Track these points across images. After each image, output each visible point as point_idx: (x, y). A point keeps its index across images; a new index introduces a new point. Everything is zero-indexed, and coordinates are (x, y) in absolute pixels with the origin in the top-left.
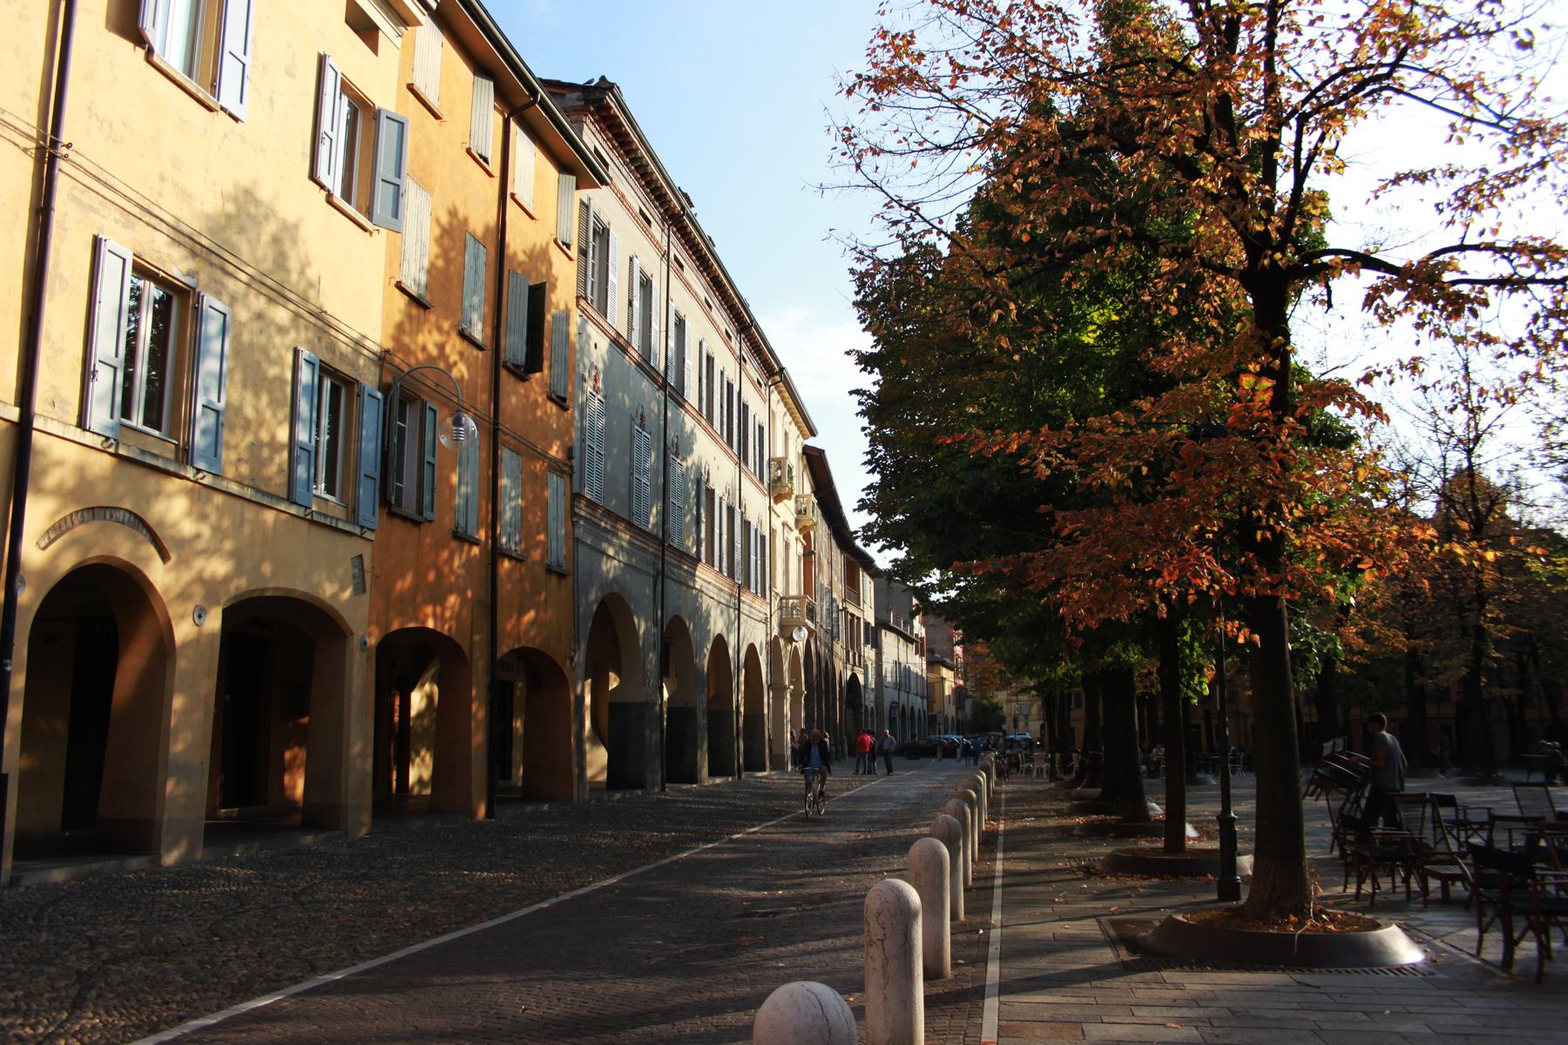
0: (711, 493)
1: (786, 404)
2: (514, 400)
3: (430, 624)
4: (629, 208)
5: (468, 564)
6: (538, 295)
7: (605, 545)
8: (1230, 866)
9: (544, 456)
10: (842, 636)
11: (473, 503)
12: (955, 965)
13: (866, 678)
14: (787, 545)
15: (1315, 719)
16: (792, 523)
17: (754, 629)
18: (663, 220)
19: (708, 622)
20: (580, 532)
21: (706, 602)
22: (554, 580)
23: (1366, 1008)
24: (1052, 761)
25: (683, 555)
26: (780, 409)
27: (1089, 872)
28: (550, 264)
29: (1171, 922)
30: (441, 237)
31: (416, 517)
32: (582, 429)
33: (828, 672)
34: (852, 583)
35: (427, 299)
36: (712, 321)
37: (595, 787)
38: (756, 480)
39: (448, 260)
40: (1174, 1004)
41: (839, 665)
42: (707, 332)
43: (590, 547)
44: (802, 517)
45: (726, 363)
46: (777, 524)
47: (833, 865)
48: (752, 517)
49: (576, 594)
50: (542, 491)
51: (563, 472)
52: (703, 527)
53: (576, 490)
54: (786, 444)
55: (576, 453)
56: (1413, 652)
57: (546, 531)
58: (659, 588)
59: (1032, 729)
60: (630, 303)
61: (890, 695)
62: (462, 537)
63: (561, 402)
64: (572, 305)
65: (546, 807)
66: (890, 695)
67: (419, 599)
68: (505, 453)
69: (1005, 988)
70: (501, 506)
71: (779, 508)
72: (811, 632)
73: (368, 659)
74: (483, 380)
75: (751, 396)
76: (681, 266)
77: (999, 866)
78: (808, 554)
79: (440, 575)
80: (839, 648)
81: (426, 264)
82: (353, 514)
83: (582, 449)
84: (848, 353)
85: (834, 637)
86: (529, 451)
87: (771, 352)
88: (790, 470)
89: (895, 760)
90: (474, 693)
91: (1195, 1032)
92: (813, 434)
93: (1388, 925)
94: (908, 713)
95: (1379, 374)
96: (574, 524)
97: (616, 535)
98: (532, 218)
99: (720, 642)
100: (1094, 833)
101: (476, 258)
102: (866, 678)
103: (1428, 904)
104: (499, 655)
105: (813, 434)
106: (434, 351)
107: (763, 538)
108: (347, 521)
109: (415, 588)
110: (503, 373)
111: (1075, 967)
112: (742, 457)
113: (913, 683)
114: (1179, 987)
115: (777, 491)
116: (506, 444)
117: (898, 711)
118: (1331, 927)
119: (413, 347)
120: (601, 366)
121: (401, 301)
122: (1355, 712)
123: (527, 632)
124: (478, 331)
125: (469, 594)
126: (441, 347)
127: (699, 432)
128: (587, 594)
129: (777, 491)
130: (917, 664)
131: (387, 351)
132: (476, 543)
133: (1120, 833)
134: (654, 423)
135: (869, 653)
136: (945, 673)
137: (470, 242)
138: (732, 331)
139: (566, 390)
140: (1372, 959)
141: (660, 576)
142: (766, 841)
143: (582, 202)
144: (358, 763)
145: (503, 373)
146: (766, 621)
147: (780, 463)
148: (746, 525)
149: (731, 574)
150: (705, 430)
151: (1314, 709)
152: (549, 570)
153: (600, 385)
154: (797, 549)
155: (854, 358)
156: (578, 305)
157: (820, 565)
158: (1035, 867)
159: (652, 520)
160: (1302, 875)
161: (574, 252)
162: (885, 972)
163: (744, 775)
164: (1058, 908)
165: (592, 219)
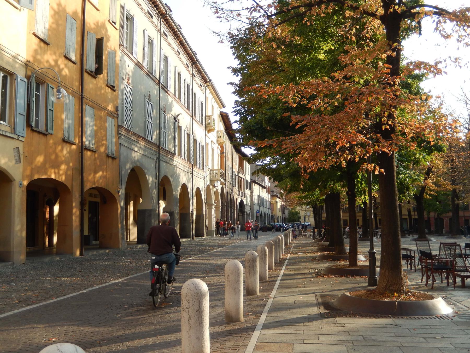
0: (180, 128)
1: (212, 95)
2: (91, 86)
3: (53, 177)
4: (143, 10)
5: (70, 152)
6: (100, 43)
7: (133, 147)
8: (373, 272)
9: (105, 109)
10: (237, 185)
11: (72, 128)
12: (245, 315)
13: (247, 202)
14: (213, 150)
15: (417, 217)
16: (215, 142)
17: (199, 182)
18: (158, 16)
19: (179, 178)
20: (122, 141)
21: (178, 170)
22: (110, 160)
23: (425, 336)
24: (314, 232)
25: (168, 152)
26: (210, 96)
27: (318, 274)
28: (107, 30)
29: (344, 296)
30: (54, 15)
31: (44, 132)
32: (122, 99)
33: (231, 199)
34: (241, 165)
35: (47, 41)
36: (180, 59)
37: (129, 244)
38: (200, 123)
39: (58, 25)
40: (338, 334)
41: (236, 197)
42: (178, 63)
43: (127, 147)
44: (219, 139)
45: (186, 76)
46: (209, 141)
47: (216, 273)
48: (198, 138)
49: (120, 167)
50: (104, 124)
51: (114, 116)
52: (177, 141)
53: (120, 124)
54: (213, 110)
55: (120, 109)
56: (454, 190)
57: (106, 140)
58: (158, 164)
59: (311, 221)
60: (144, 49)
61: (256, 208)
62: (66, 141)
63: (112, 88)
64: (117, 49)
65: (107, 251)
66: (256, 208)
67: (47, 166)
68: (87, 108)
69: (266, 326)
70: (85, 129)
71: (210, 135)
72: (222, 183)
73: (23, 191)
74: (76, 76)
75: (197, 90)
76: (167, 36)
77: (282, 272)
78: (222, 153)
79: (57, 156)
80: (236, 190)
81: (48, 26)
82: (14, 130)
83: (122, 108)
84: (228, 68)
85: (234, 186)
86: (98, 107)
87: (205, 73)
88: (214, 120)
89: (259, 233)
90: (74, 205)
91: (345, 348)
92: (224, 107)
93: (437, 297)
94: (263, 215)
95: (441, 62)
96: (119, 138)
97: (138, 143)
98: (98, 10)
99: (184, 187)
100: (324, 258)
101: (72, 25)
102: (247, 202)
103: (455, 287)
104: (85, 189)
105: (224, 107)
106: (53, 63)
107: (203, 146)
108: (11, 133)
109: (45, 162)
110: (86, 75)
111: (299, 316)
112: (194, 115)
113: (265, 204)
114: (343, 325)
115: (209, 128)
116: (87, 104)
117: (259, 214)
118: (412, 298)
119: (42, 60)
120: (131, 74)
121: (36, 40)
122: (432, 214)
123: (98, 181)
124: (73, 57)
125: (71, 164)
126: (56, 61)
127: (175, 103)
128: (126, 165)
129: (209, 128)
130: (267, 196)
131: (29, 62)
132: (74, 144)
133: (335, 259)
134: (155, 98)
135: (248, 192)
136: (278, 200)
137: (69, 19)
138: (189, 64)
139: (114, 82)
140: (426, 312)
141: (158, 160)
142: (193, 263)
143: (121, 6)
144: (19, 234)
145: (86, 75)
146: (205, 179)
147: (210, 117)
148: (195, 141)
149: (189, 160)
150: (177, 103)
151: (416, 213)
152: (108, 156)
153: (130, 81)
154: (217, 151)
155: (230, 70)
156: (120, 48)
157: (228, 158)
158: (296, 272)
159: (154, 137)
160: (400, 276)
161: (118, 26)
162: (189, 324)
163: (195, 238)
164: (300, 289)
165: (125, 13)
